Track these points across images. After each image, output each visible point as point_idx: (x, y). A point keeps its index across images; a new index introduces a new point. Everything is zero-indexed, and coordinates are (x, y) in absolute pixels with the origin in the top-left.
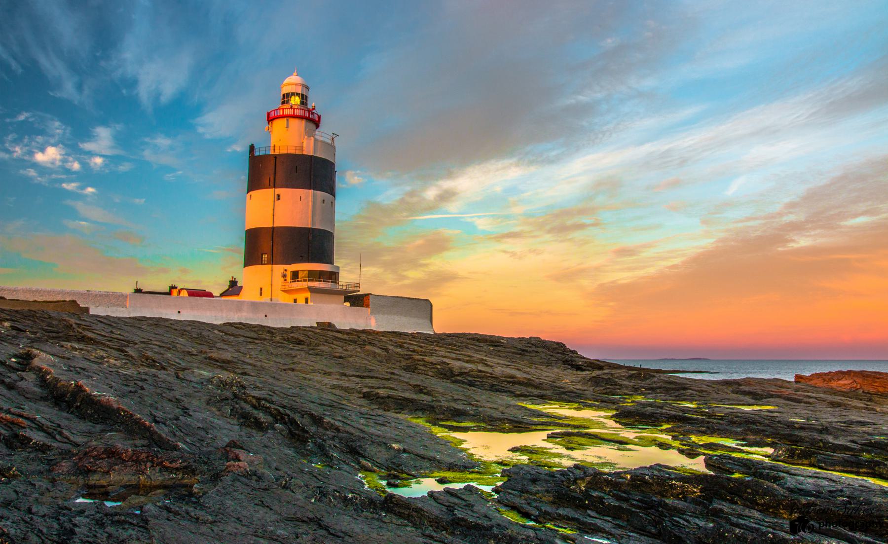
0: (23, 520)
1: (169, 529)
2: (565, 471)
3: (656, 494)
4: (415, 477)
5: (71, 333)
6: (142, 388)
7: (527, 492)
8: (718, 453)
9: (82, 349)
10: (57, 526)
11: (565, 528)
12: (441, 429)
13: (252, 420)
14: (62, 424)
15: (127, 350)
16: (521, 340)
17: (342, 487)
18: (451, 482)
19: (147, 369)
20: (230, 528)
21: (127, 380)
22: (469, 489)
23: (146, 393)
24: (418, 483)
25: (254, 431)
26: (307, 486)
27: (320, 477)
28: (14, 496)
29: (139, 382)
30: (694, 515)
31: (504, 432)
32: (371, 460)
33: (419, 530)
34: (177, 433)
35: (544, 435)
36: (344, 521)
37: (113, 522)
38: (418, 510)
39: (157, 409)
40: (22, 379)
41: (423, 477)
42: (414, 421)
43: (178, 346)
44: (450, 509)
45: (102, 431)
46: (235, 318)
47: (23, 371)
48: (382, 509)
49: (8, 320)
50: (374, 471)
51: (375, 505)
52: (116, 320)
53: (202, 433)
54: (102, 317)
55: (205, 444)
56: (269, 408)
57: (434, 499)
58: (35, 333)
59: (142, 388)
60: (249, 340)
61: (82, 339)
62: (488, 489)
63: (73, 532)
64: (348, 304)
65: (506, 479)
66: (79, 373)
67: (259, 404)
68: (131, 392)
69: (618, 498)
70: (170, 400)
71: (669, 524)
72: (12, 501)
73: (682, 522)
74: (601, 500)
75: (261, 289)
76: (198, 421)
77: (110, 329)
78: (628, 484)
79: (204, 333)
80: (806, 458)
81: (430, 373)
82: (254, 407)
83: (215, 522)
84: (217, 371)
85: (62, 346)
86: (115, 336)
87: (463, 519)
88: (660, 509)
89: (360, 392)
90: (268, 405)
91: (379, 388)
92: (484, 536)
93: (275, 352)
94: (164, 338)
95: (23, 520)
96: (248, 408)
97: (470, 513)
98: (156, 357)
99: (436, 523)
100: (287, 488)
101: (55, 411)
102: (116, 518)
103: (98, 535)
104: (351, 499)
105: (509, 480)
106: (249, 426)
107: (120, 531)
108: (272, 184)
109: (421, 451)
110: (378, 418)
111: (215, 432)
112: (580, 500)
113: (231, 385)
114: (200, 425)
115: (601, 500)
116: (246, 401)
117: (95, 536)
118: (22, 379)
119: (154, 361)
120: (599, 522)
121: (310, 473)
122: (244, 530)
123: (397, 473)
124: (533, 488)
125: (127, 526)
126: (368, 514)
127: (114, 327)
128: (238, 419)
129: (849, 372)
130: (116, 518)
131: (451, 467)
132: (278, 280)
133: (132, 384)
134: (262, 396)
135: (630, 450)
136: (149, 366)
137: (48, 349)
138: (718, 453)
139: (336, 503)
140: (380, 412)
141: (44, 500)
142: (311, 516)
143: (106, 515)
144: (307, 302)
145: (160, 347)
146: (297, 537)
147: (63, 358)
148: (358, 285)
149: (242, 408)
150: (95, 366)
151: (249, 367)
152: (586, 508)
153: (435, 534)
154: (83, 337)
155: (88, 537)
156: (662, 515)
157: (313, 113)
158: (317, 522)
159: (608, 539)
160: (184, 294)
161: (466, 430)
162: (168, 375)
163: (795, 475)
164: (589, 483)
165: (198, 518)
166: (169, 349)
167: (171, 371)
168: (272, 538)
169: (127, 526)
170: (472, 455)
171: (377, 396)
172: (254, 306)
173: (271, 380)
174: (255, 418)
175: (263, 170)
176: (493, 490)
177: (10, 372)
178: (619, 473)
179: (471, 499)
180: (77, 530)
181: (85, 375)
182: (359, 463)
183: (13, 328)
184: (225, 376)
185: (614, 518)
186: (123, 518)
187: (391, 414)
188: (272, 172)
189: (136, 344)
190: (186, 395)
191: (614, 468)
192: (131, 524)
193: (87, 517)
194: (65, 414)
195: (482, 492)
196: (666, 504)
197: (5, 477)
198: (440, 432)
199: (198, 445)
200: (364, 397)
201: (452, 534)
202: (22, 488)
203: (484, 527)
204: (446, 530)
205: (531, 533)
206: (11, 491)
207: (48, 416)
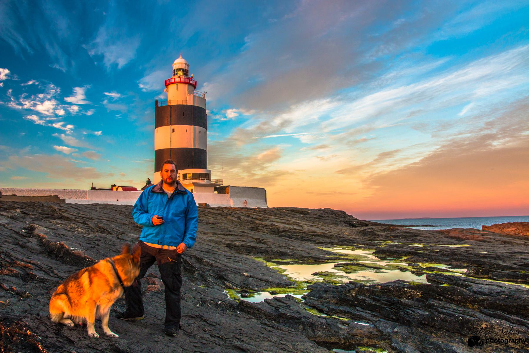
5: (56, 215)
6: (98, 245)
7: (322, 298)
9: (62, 224)
12: (272, 264)
14: (53, 267)
17: (215, 298)
18: (278, 294)
19: (100, 234)
22: (288, 297)
23: (100, 248)
26: (194, 298)
27: (202, 293)
29: (96, 242)
30: (417, 308)
31: (309, 264)
33: (259, 321)
35: (332, 265)
36: (216, 317)
40: (29, 242)
43: (118, 220)
44: (277, 309)
48: (238, 309)
49: (18, 208)
50: (233, 289)
54: (73, 204)
57: (268, 303)
58: (35, 215)
59: (98, 245)
61: (62, 218)
62: (299, 297)
64: (216, 192)
65: (310, 291)
66: (61, 237)
68: (91, 247)
69: (374, 300)
71: (403, 313)
73: (410, 312)
74: (364, 301)
77: (78, 211)
80: (486, 274)
86: (81, 215)
87: (284, 314)
89: (224, 244)
91: (235, 241)
97: (288, 310)
98: (105, 227)
99: (269, 317)
101: (49, 259)
104: (220, 304)
108: (169, 123)
109: (260, 276)
112: (352, 302)
115: (364, 301)
118: (29, 242)
119: (104, 229)
120: (363, 314)
121: (196, 290)
123: (247, 289)
124: (325, 296)
127: (80, 210)
131: (278, 285)
133: (92, 243)
135: (383, 272)
140: (237, 255)
142: (197, 314)
145: (107, 221)
147: (52, 229)
148: (222, 181)
150: (70, 233)
152: (355, 306)
153: (268, 323)
154: (63, 216)
156: (399, 308)
157: (192, 80)
159: (368, 323)
160: (120, 189)
161: (287, 264)
162: (113, 237)
164: (357, 291)
166: (113, 222)
167: (114, 235)
170: (290, 278)
171: (235, 246)
175: (165, 115)
176: (302, 297)
181: (64, 238)
182: (224, 284)
183: (22, 212)
187: (244, 256)
188: (169, 115)
189: (93, 219)
194: (54, 261)
195: (296, 298)
196: (401, 302)
200: (227, 246)
201: (278, 322)
202: (33, 303)
204: (275, 320)
206: (27, 305)
207: (44, 262)
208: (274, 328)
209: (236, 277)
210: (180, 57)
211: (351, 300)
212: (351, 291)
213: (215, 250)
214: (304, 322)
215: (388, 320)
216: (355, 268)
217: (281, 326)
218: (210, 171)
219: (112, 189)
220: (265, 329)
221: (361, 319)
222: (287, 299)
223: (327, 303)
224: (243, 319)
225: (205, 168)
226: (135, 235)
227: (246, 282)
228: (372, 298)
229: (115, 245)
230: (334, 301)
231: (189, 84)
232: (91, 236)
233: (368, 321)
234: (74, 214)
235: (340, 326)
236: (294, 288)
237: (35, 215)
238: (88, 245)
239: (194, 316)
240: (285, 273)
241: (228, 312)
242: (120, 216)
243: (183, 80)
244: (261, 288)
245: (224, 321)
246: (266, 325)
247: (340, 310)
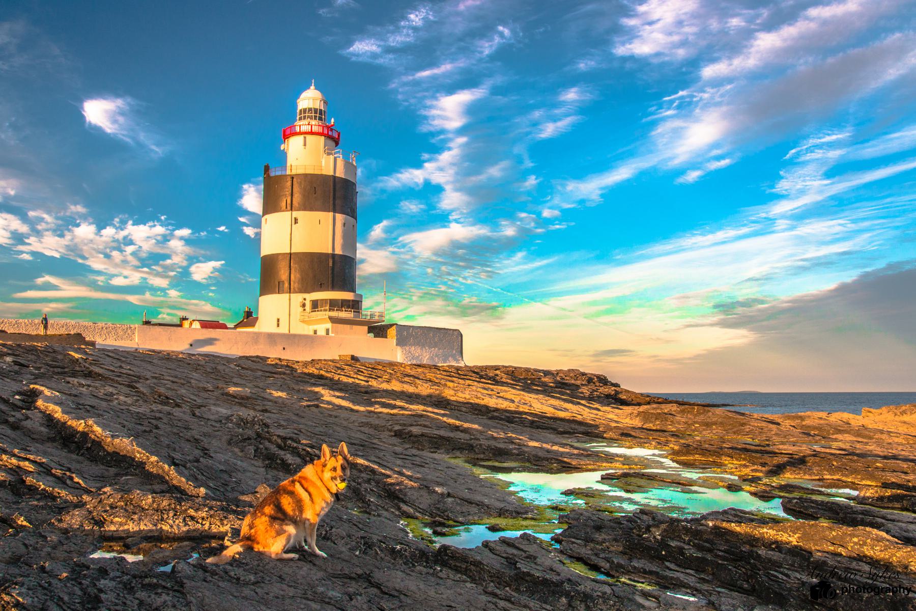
0: (40, 586)
1: (207, 593)
2: (630, 517)
3: (744, 543)
4: (462, 524)
5: (78, 369)
6: (157, 427)
7: (592, 541)
8: (796, 495)
9: (89, 386)
10: (80, 593)
11: (643, 583)
12: (483, 470)
13: (279, 461)
14: (72, 468)
15: (137, 385)
16: (527, 370)
17: (385, 537)
18: (504, 530)
19: (160, 407)
20: (275, 589)
21: (139, 418)
22: (525, 537)
23: (161, 433)
24: (468, 530)
25: (281, 473)
26: (349, 536)
27: (360, 526)
28: (23, 550)
29: (153, 421)
30: (792, 567)
31: (551, 473)
32: (412, 505)
33: (479, 587)
34: (200, 477)
35: (597, 475)
36: (396, 578)
37: (143, 586)
38: (477, 564)
39: (174, 450)
40: (27, 418)
41: (472, 524)
42: (453, 461)
43: (193, 381)
44: (511, 562)
45: (117, 475)
46: (252, 352)
47: (28, 409)
48: (436, 562)
49: (9, 354)
50: (417, 518)
51: (427, 558)
52: (125, 354)
53: (226, 476)
54: (109, 351)
55: (229, 489)
56: (296, 448)
57: (490, 550)
58: (39, 368)
59: (157, 427)
60: (268, 374)
61: (89, 375)
62: (546, 537)
63: (98, 600)
64: (372, 335)
65: (565, 526)
66: (88, 411)
67: (285, 444)
68: (145, 431)
69: (699, 548)
70: (188, 440)
71: (765, 578)
72: (21, 557)
73: (780, 576)
74: (681, 550)
75: (278, 320)
76: (220, 463)
77: (119, 364)
78: (711, 533)
79: (219, 367)
80: (898, 502)
81: (464, 409)
82: (279, 447)
83: (258, 582)
84: (236, 408)
85: (68, 382)
86: (125, 371)
87: (528, 574)
88: (752, 561)
89: (390, 431)
90: (295, 445)
91: (411, 425)
92: (554, 593)
93: (296, 387)
94: (177, 373)
95: (40, 586)
96: (273, 448)
97: (533, 565)
98: (169, 394)
99: (497, 578)
100: (328, 539)
101: (64, 453)
102: (147, 581)
103: (128, 602)
104: (399, 551)
105: (569, 527)
106: (275, 468)
107: (153, 596)
108: (289, 208)
109: (466, 494)
110: (414, 458)
111: (239, 475)
112: (656, 550)
113: (253, 423)
114: (222, 468)
115: (681, 550)
116: (270, 441)
117: (125, 603)
118: (27, 418)
119: (167, 398)
120: (682, 577)
121: (350, 521)
122: (291, 592)
123: (441, 521)
124: (599, 537)
125: (160, 591)
126: (422, 568)
127: (123, 362)
128: (263, 460)
129: (402, 392)
130: (147, 581)
131: (501, 513)
132: (297, 309)
133: (146, 423)
134: (289, 436)
135: (696, 492)
136: (162, 403)
137: (54, 385)
138: (796, 495)
139: (383, 555)
140: (414, 451)
141: (58, 555)
142: (360, 572)
143: (134, 577)
144: (328, 333)
145: (173, 382)
146: (351, 599)
147: (70, 395)
149: (266, 449)
150: (104, 404)
151: (270, 403)
152: (663, 559)
153: (498, 592)
154: (90, 372)
155: (116, 605)
156: (754, 567)
157: (332, 130)
158: (367, 579)
159: (694, 595)
160: (196, 325)
161: (508, 470)
162: (184, 413)
163: (894, 521)
164: (665, 530)
165: (238, 579)
166: (183, 384)
167: (186, 408)
168: (324, 601)
169: (160, 591)
170: (522, 499)
171: (410, 434)
172: (272, 338)
173: (294, 418)
174: (282, 460)
176: (552, 539)
177: (14, 410)
178: (697, 520)
179: (532, 549)
180: (103, 596)
181: (95, 413)
182: (399, 509)
183: (16, 363)
184: (244, 413)
185: (697, 571)
186: (155, 581)
187: (426, 454)
188: (288, 193)
189: (147, 379)
190: (205, 435)
191: (683, 513)
192: (164, 587)
193: (113, 579)
194: (74, 456)
195: (541, 541)
196: (759, 556)
197: (12, 527)
198: (484, 474)
199: (222, 490)
200: (395, 436)
201: (517, 590)
202: (31, 541)
203: (553, 582)
204: (509, 586)
205: (608, 590)
206: (20, 544)
207: (56, 459)
208: (513, 603)
209: (421, 496)
210: (313, 87)
211: (653, 548)
212: (653, 529)
213: (375, 441)
214: (570, 592)
215: (731, 590)
216: (642, 482)
217: (524, 599)
218: (361, 296)
219: (181, 325)
220: (495, 604)
221: (678, 586)
222: (526, 542)
223: (603, 550)
224: (449, 582)
225: (352, 289)
226: (224, 411)
227: (440, 506)
228: (694, 545)
229: (187, 428)
230: (617, 547)
231: (328, 137)
232: (143, 409)
233: (695, 591)
234: (112, 368)
235: (641, 600)
236: (532, 519)
237: (39, 368)
238: (140, 427)
239: (353, 575)
240: (512, 489)
241: (418, 568)
242: (195, 375)
243: (315, 129)
244: (471, 518)
245: (413, 588)
246: (495, 595)
247: (635, 568)
